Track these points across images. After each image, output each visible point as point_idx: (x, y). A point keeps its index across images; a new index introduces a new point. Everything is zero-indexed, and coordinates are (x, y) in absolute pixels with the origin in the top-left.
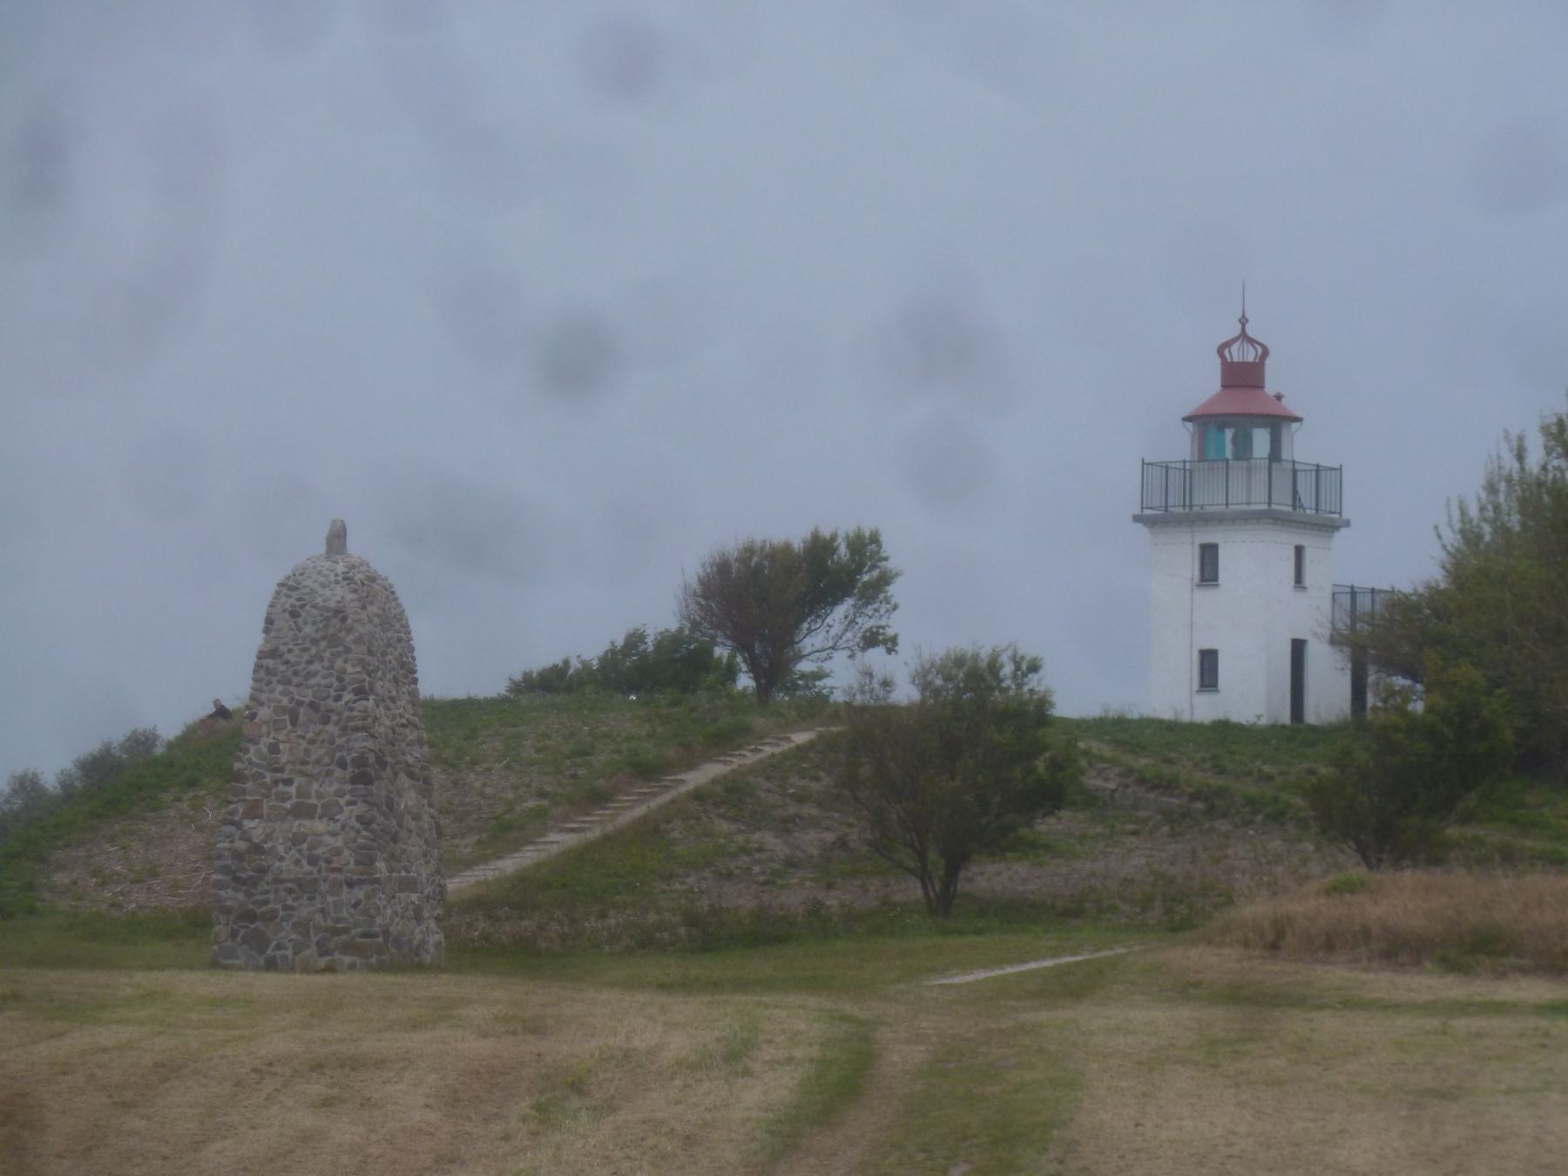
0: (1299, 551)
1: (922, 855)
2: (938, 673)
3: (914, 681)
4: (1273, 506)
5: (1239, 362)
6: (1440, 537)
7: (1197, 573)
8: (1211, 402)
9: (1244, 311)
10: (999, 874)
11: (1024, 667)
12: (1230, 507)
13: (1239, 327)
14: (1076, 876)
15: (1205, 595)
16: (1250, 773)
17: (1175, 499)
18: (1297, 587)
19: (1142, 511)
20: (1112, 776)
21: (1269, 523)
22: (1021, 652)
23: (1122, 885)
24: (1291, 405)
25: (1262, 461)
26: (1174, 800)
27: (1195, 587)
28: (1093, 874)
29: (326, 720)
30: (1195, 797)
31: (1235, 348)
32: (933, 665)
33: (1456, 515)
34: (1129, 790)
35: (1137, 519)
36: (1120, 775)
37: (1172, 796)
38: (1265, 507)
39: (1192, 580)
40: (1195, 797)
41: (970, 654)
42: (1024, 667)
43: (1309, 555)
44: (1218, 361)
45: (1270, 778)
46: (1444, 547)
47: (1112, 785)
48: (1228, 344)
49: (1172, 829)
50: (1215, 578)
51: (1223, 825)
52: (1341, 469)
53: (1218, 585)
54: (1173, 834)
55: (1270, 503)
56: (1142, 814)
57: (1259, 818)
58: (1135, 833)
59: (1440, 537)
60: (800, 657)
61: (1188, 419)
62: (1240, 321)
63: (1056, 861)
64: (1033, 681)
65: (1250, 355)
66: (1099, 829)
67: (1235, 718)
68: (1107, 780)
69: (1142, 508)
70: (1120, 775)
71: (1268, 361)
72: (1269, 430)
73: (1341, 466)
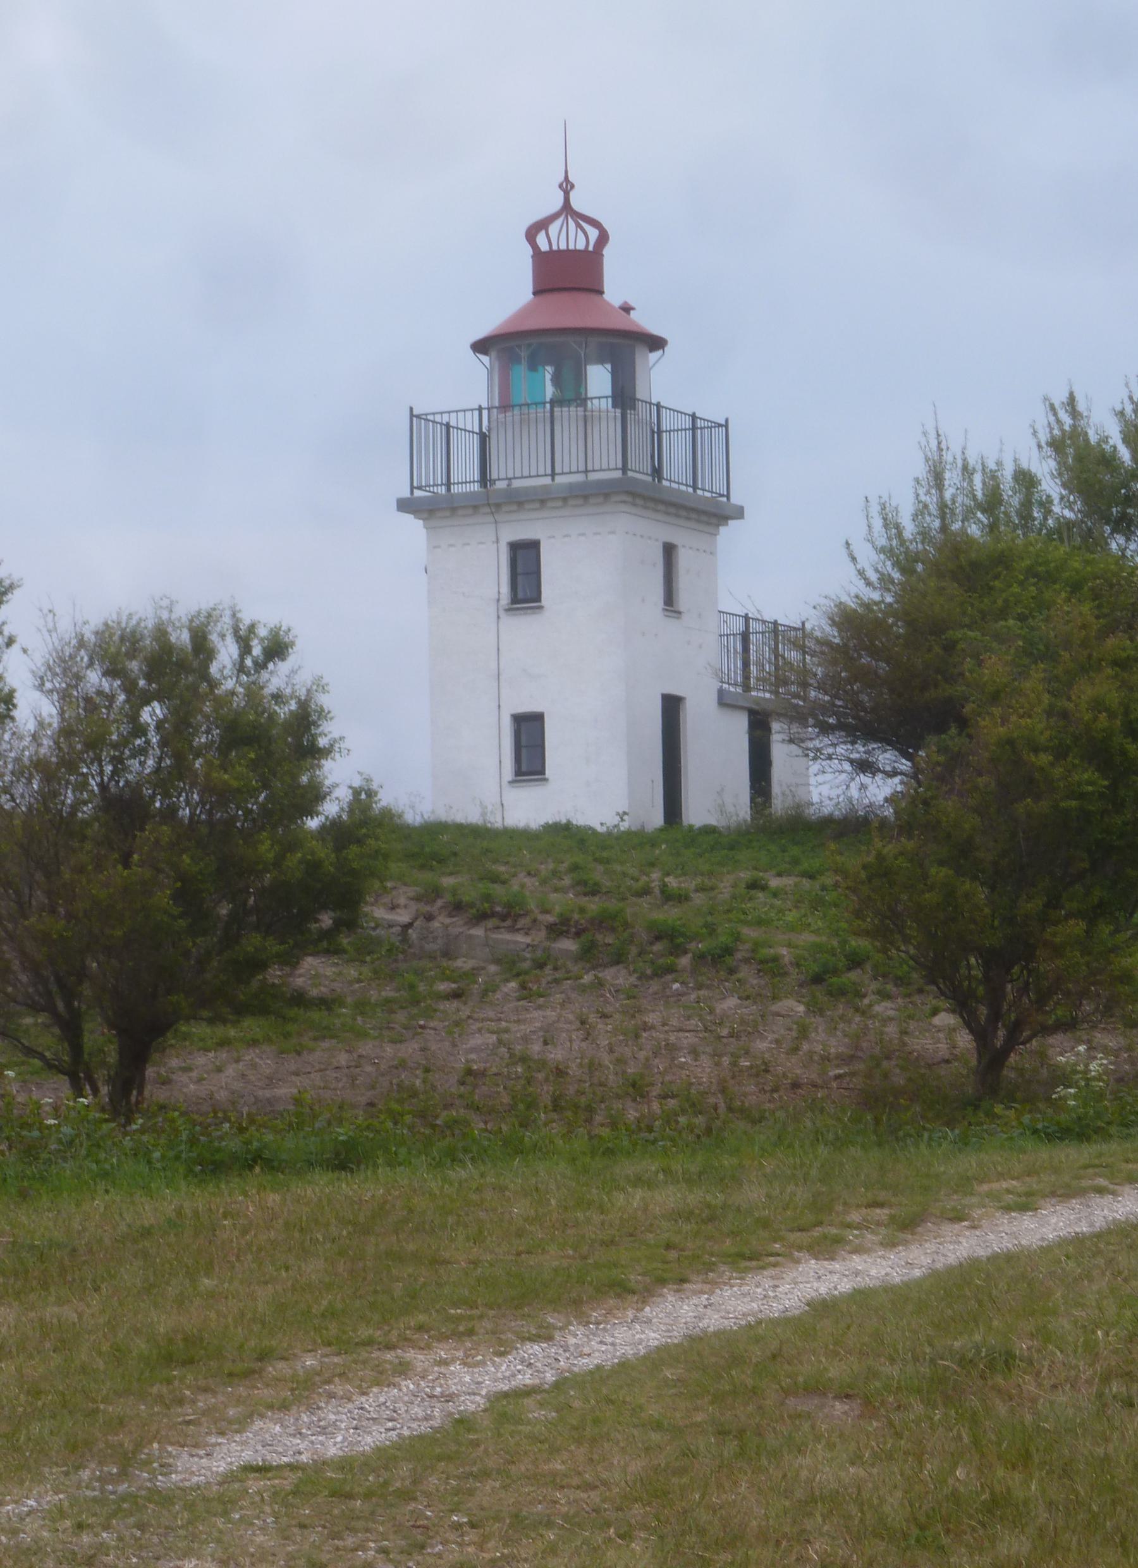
0: (669, 550)
1: (71, 1029)
2: (91, 659)
3: (43, 684)
4: (630, 474)
5: (568, 250)
6: (854, 559)
7: (505, 589)
8: (526, 312)
9: (566, 172)
10: (219, 1070)
11: (257, 651)
12: (559, 479)
13: (560, 195)
14: (369, 1069)
15: (521, 627)
16: (646, 892)
17: (466, 470)
18: (667, 610)
19: (412, 493)
20: (402, 901)
21: (624, 502)
22: (246, 619)
23: (462, 1083)
24: (645, 320)
25: (603, 401)
26: (520, 938)
27: (502, 613)
28: (402, 1065)
29: (899, 1435)
30: (557, 930)
31: (554, 229)
32: (82, 643)
33: (878, 523)
34: (436, 924)
35: (404, 505)
36: (417, 899)
37: (513, 929)
38: (618, 474)
39: (498, 600)
40: (557, 930)
41: (150, 624)
42: (257, 651)
43: (685, 559)
44: (529, 251)
45: (681, 898)
46: (861, 573)
47: (403, 917)
48: (541, 225)
49: (523, 986)
50: (538, 598)
51: (617, 977)
52: (726, 426)
53: (541, 607)
54: (526, 993)
55: (624, 469)
56: (463, 964)
57: (685, 961)
58: (457, 995)
59: (854, 559)
60: (258, 1464)
61: (481, 347)
62: (561, 186)
63: (326, 1044)
64: (277, 677)
65: (580, 241)
66: (388, 993)
67: (579, 820)
68: (393, 908)
69: (412, 488)
70: (417, 899)
71: (606, 252)
72: (609, 366)
73: (727, 420)
